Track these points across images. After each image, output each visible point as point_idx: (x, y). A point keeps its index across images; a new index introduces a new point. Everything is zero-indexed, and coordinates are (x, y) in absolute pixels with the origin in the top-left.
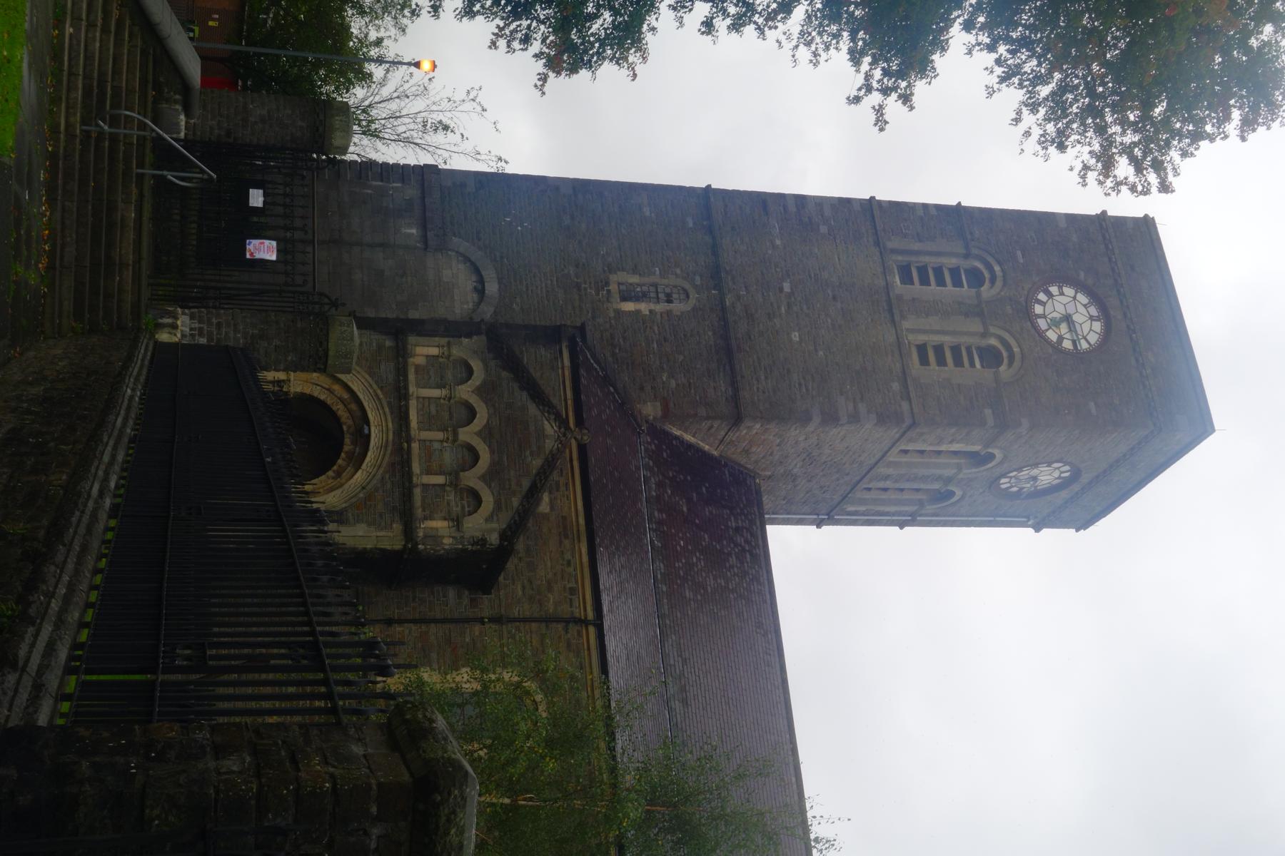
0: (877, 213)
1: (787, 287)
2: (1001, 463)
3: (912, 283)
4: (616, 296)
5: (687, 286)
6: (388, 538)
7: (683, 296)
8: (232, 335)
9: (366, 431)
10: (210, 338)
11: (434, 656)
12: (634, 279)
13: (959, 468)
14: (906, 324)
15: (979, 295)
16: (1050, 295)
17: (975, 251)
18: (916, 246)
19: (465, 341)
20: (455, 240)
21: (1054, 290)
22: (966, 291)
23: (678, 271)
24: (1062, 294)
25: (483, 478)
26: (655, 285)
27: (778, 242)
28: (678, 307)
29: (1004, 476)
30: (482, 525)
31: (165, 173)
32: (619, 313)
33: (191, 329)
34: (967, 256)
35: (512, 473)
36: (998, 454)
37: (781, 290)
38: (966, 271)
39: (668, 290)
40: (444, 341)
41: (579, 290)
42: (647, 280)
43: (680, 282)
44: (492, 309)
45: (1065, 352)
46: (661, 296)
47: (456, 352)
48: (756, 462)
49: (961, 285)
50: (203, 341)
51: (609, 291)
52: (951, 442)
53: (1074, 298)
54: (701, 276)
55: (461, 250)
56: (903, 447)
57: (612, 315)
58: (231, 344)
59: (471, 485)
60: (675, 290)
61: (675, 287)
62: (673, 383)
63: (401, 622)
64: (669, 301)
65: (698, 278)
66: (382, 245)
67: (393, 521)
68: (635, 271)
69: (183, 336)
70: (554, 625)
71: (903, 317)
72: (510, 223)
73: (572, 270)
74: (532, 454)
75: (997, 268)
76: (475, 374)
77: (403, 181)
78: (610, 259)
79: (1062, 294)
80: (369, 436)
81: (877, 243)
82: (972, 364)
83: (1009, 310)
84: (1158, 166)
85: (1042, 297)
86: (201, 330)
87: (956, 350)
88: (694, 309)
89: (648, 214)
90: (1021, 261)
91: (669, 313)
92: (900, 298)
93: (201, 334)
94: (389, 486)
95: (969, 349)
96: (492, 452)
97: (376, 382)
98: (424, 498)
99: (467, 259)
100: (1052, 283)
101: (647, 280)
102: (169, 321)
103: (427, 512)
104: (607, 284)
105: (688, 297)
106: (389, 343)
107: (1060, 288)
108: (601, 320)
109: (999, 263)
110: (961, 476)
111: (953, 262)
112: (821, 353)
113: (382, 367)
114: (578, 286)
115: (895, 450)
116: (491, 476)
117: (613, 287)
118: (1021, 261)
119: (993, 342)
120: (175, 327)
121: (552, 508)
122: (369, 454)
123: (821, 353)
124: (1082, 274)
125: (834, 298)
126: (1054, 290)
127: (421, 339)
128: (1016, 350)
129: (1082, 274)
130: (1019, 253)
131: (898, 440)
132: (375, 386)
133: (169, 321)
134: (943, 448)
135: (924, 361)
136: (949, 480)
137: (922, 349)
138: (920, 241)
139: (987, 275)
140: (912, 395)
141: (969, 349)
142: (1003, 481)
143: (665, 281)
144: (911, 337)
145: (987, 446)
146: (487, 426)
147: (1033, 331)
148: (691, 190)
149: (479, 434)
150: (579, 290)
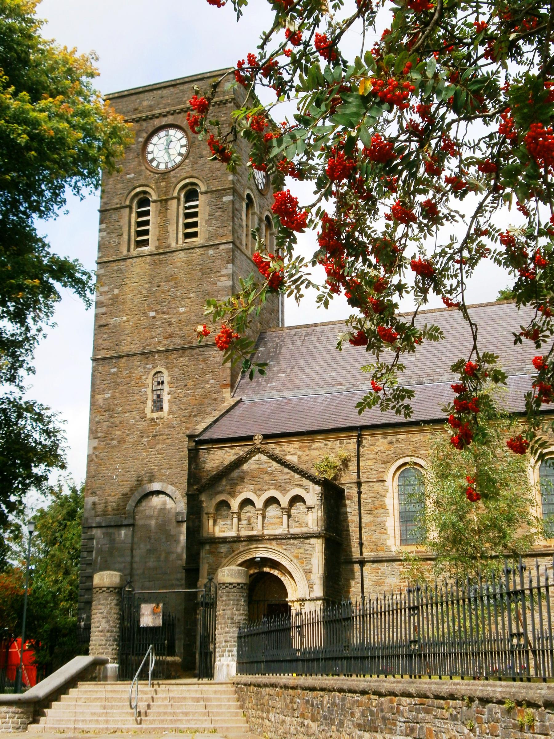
0: (106, 259)
1: (152, 314)
2: (251, 190)
3: (148, 240)
4: (160, 414)
5: (153, 372)
6: (318, 545)
7: (159, 375)
8: (231, 635)
9: (259, 559)
10: (234, 646)
11: (379, 519)
12: (149, 403)
13: (254, 214)
14: (173, 245)
15: (154, 202)
16: (153, 159)
17: (128, 203)
18: (125, 237)
19: (204, 505)
20: (128, 508)
21: (150, 157)
22: (151, 208)
23: (144, 377)
24: (152, 152)
25: (284, 494)
26: (153, 391)
27: (125, 318)
28: (166, 378)
29: (257, 186)
30: (312, 494)
31: (150, 672)
32: (170, 413)
33: (229, 656)
34: (130, 207)
35: (280, 478)
36: (248, 191)
37: (154, 317)
38: (139, 208)
39: (156, 384)
40: (205, 516)
41: (156, 436)
42: (150, 397)
43: (150, 376)
44: (169, 486)
45: (188, 152)
46: (159, 387)
47: (212, 510)
48: (253, 332)
49: (149, 211)
50: (235, 649)
51: (157, 418)
52: (241, 219)
53: (155, 145)
54: (147, 364)
55: (134, 504)
56: (245, 247)
57: (171, 416)
58: (236, 635)
59: (288, 500)
60: (155, 379)
61: (153, 379)
62: (212, 381)
63: (361, 538)
64: (162, 383)
65: (148, 366)
66: (132, 551)
67: (310, 544)
68: (144, 403)
69: (233, 660)
70: (361, 453)
71: (169, 246)
72: (117, 476)
73: (145, 439)
74: (270, 467)
75: (138, 190)
76: (224, 498)
77: (93, 539)
78: (138, 417)
79: (152, 152)
80: (261, 558)
81: (124, 260)
82: (196, 206)
83: (163, 184)
84: (534, 326)
85: (154, 164)
86: (229, 651)
87: (187, 216)
88: (167, 368)
89: (109, 395)
90: (133, 175)
91: (169, 383)
92: (158, 248)
93: (231, 651)
94: (289, 546)
95: (187, 208)
96: (269, 489)
97: (230, 554)
98: (297, 527)
99: (140, 501)
100: (145, 158)
101: (150, 397)
102: (225, 667)
103: (303, 525)
104: (153, 419)
105: (159, 372)
106: (207, 547)
107: (149, 153)
108: (175, 423)
109: (135, 188)
110: (258, 213)
111: (134, 215)
112: (192, 295)
113: (222, 551)
114: (155, 436)
115: (246, 252)
116: (281, 488)
117: (155, 415)
118: (133, 175)
119: (182, 195)
120: (228, 666)
121: (295, 454)
122: (271, 557)
123: (192, 295)
124: (140, 140)
125: (158, 286)
126: (150, 157)
127: (205, 529)
128: (187, 181)
129: (140, 140)
130: (128, 176)
131: (241, 250)
132: (233, 555)
133: (225, 667)
134: (244, 224)
135: (195, 235)
136: (260, 220)
137: (187, 236)
138: (122, 235)
139: (141, 196)
140: (216, 242)
141: (187, 208)
142: (260, 188)
143: (150, 385)
144: (180, 242)
145: (243, 199)
146: (255, 491)
147: (176, 170)
148: (95, 370)
149: (259, 496)
150: (156, 436)
